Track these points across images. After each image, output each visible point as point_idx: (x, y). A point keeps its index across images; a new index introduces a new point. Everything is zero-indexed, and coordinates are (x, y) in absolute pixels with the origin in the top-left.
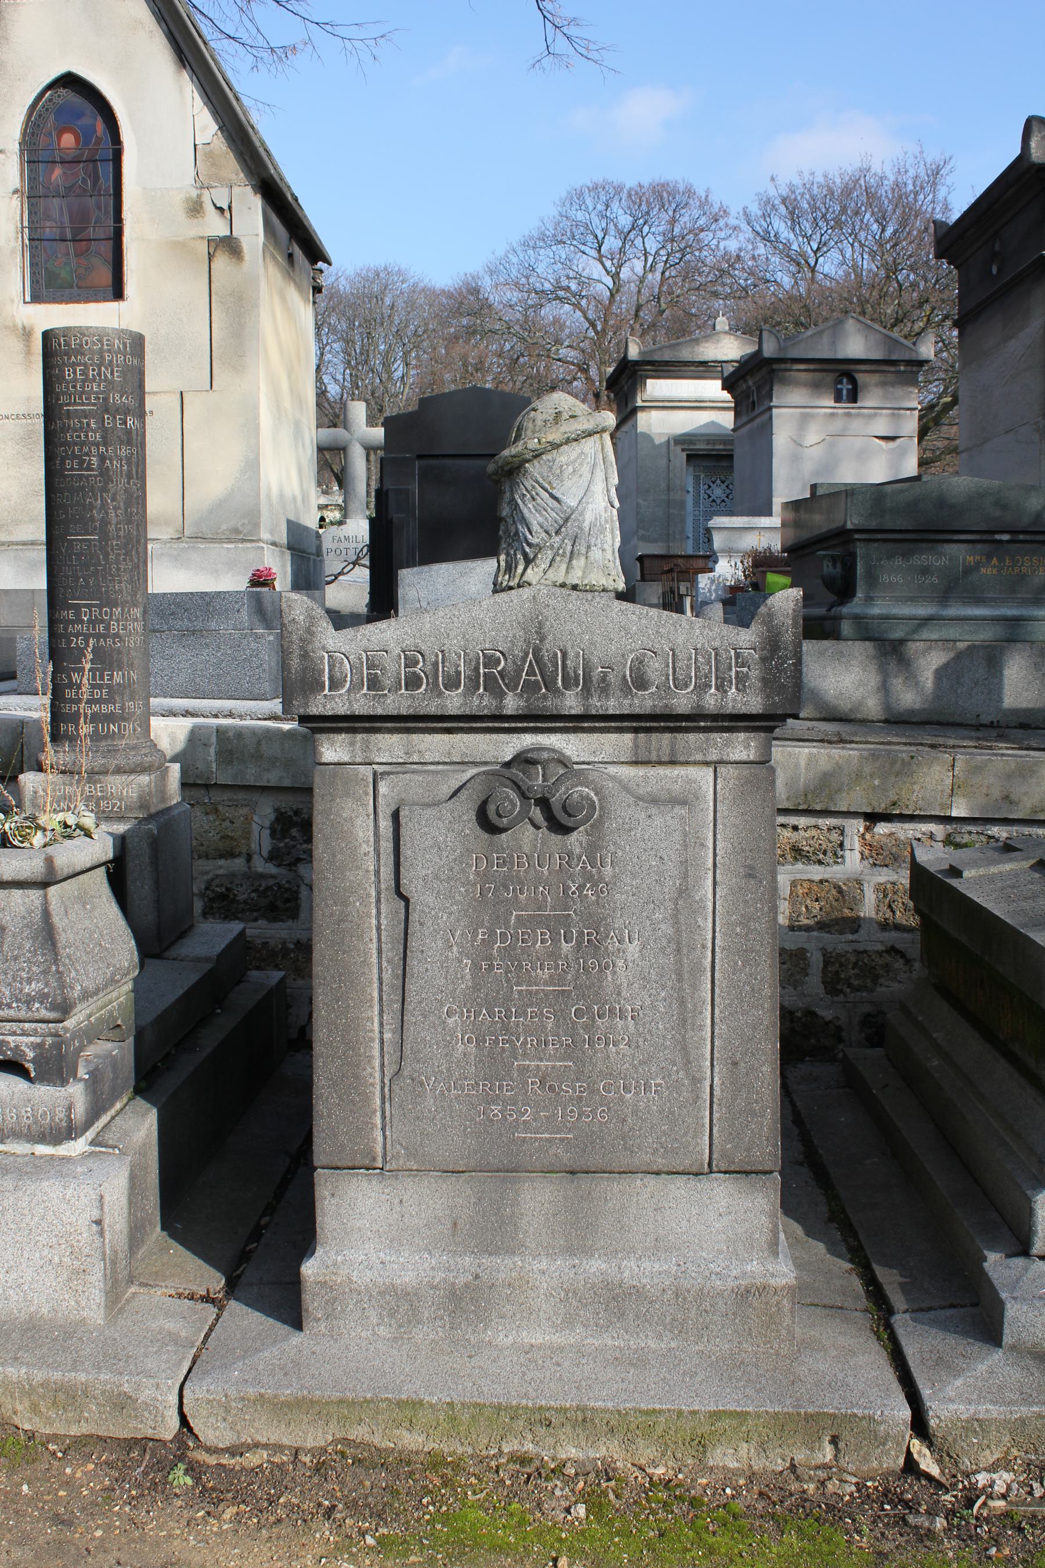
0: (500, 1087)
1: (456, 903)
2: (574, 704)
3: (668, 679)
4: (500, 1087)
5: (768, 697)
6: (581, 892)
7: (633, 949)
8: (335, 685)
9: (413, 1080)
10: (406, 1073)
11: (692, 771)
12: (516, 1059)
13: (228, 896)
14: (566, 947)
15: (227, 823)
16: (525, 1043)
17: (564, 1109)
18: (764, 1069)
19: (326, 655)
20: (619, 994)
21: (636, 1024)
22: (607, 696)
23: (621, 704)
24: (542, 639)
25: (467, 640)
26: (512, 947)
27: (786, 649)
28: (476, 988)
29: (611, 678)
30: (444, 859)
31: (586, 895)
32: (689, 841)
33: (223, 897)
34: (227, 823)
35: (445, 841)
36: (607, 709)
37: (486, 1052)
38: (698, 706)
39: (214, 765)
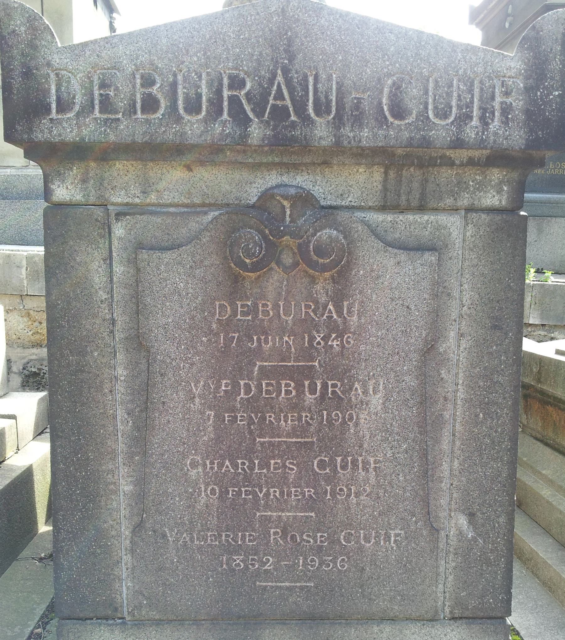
0: (243, 537)
1: (197, 353)
2: (324, 134)
3: (426, 108)
4: (243, 537)
5: (531, 131)
6: (326, 343)
7: (376, 401)
8: (62, 107)
9: (154, 531)
10: (148, 525)
11: (443, 219)
12: (258, 510)
13: (39, 374)
14: (309, 398)
15: (36, 324)
16: (267, 494)
17: (305, 559)
18: (501, 520)
19: (52, 76)
20: (361, 446)
21: (377, 476)
22: (361, 126)
23: (375, 135)
24: (292, 58)
25: (208, 58)
26: (256, 398)
27: (552, 78)
28: (218, 439)
29: (366, 105)
30: (185, 307)
31: (332, 346)
32: (439, 292)
33: (35, 374)
34: (36, 324)
35: (186, 288)
36: (360, 141)
37: (228, 504)
38: (458, 139)
39: (25, 282)
